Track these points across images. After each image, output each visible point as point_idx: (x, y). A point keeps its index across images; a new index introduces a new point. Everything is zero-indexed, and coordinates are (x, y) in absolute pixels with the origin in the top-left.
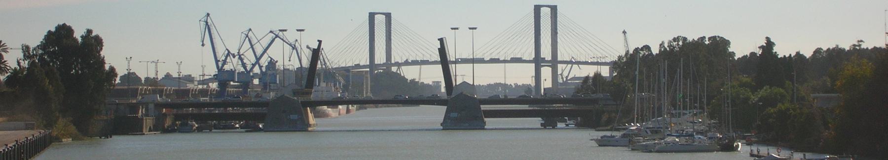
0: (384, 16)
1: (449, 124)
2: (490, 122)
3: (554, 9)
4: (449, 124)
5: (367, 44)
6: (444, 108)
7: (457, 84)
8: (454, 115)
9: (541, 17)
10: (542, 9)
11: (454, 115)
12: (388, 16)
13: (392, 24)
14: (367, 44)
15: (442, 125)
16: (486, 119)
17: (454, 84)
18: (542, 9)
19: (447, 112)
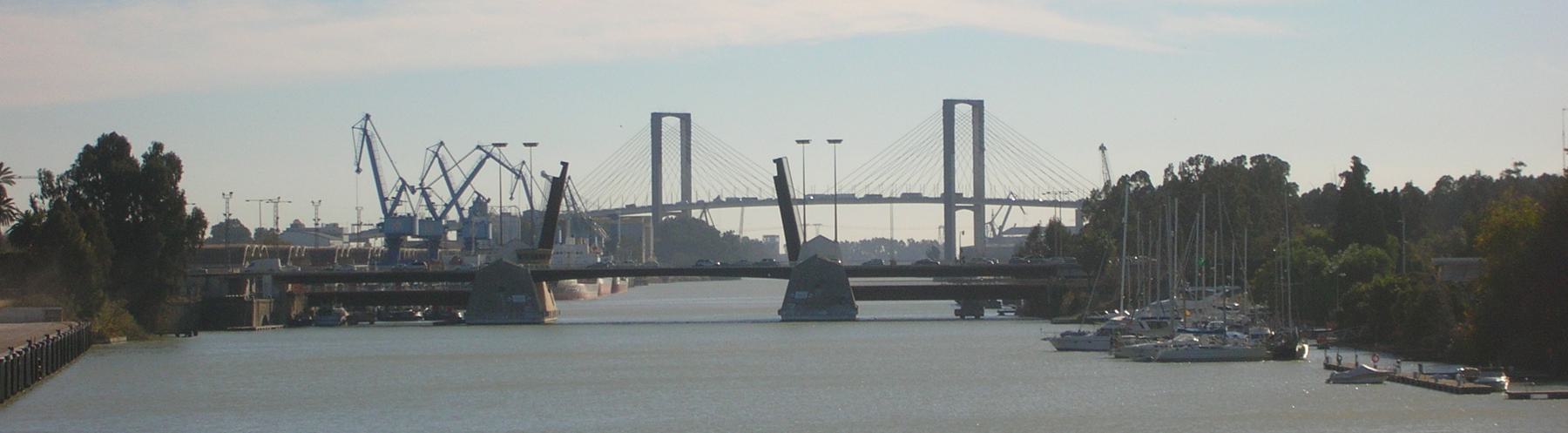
0: (678, 120)
1: (795, 311)
2: (865, 308)
3: (978, 107)
4: (795, 311)
5: (648, 169)
6: (782, 284)
7: (807, 240)
8: (801, 295)
9: (956, 122)
10: (956, 106)
11: (801, 295)
12: (685, 119)
13: (692, 134)
14: (648, 169)
15: (780, 312)
16: (858, 303)
17: (802, 240)
18: (956, 106)
19: (790, 290)
